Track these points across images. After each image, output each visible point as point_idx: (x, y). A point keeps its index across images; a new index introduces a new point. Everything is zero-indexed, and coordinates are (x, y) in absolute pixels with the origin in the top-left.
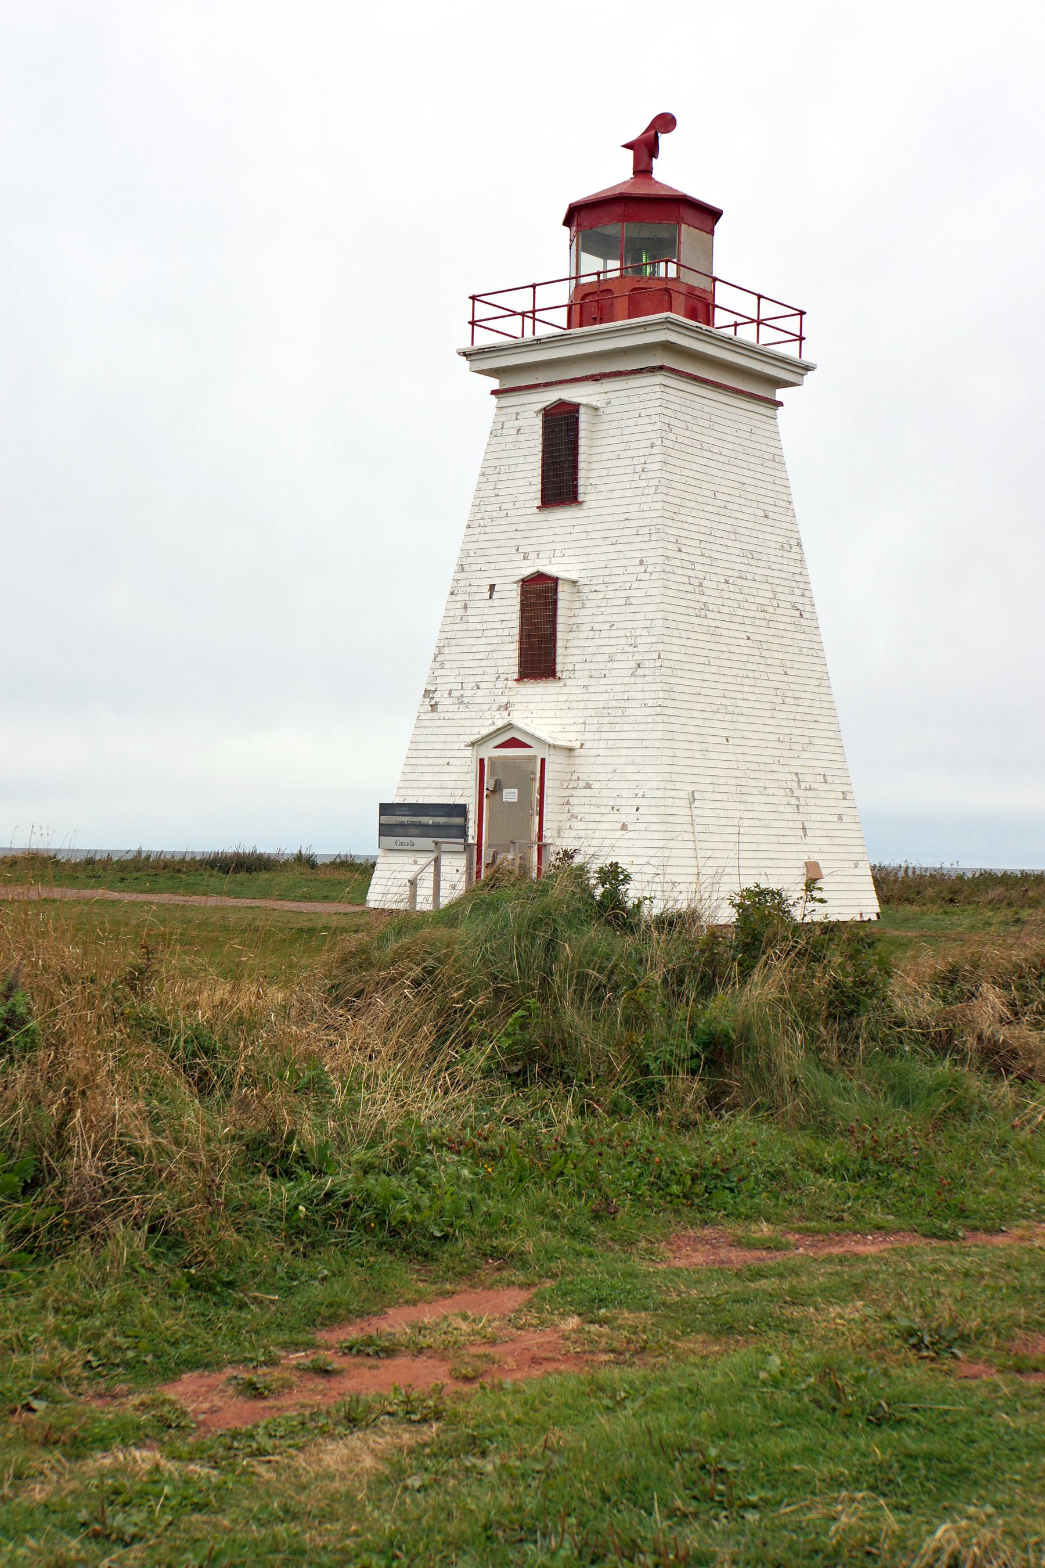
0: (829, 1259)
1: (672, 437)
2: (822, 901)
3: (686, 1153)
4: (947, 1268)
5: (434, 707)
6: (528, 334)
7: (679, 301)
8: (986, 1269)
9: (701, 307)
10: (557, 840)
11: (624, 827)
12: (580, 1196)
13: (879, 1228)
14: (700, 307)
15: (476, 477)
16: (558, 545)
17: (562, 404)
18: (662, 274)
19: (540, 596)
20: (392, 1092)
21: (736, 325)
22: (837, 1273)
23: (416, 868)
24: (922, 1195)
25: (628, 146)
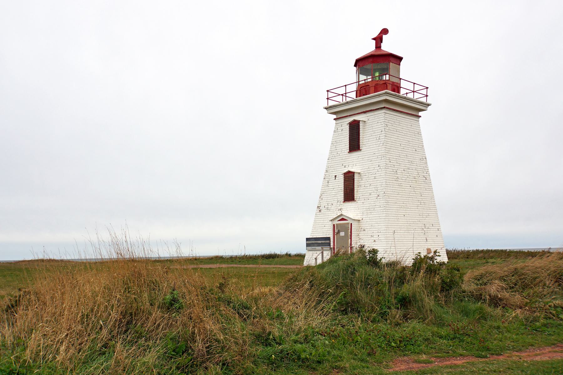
0: (447, 367)
1: (388, 128)
2: (439, 256)
3: (398, 333)
4: (488, 369)
5: (320, 211)
6: (344, 101)
7: (390, 86)
8: (501, 370)
9: (396, 88)
10: (356, 244)
11: (375, 241)
12: (364, 348)
13: (461, 355)
14: (396, 88)
15: (330, 145)
16: (355, 163)
17: (355, 121)
18: (384, 79)
19: (349, 177)
20: (305, 318)
21: (407, 93)
22: (450, 372)
23: (317, 255)
24: (474, 344)
25: (373, 39)
